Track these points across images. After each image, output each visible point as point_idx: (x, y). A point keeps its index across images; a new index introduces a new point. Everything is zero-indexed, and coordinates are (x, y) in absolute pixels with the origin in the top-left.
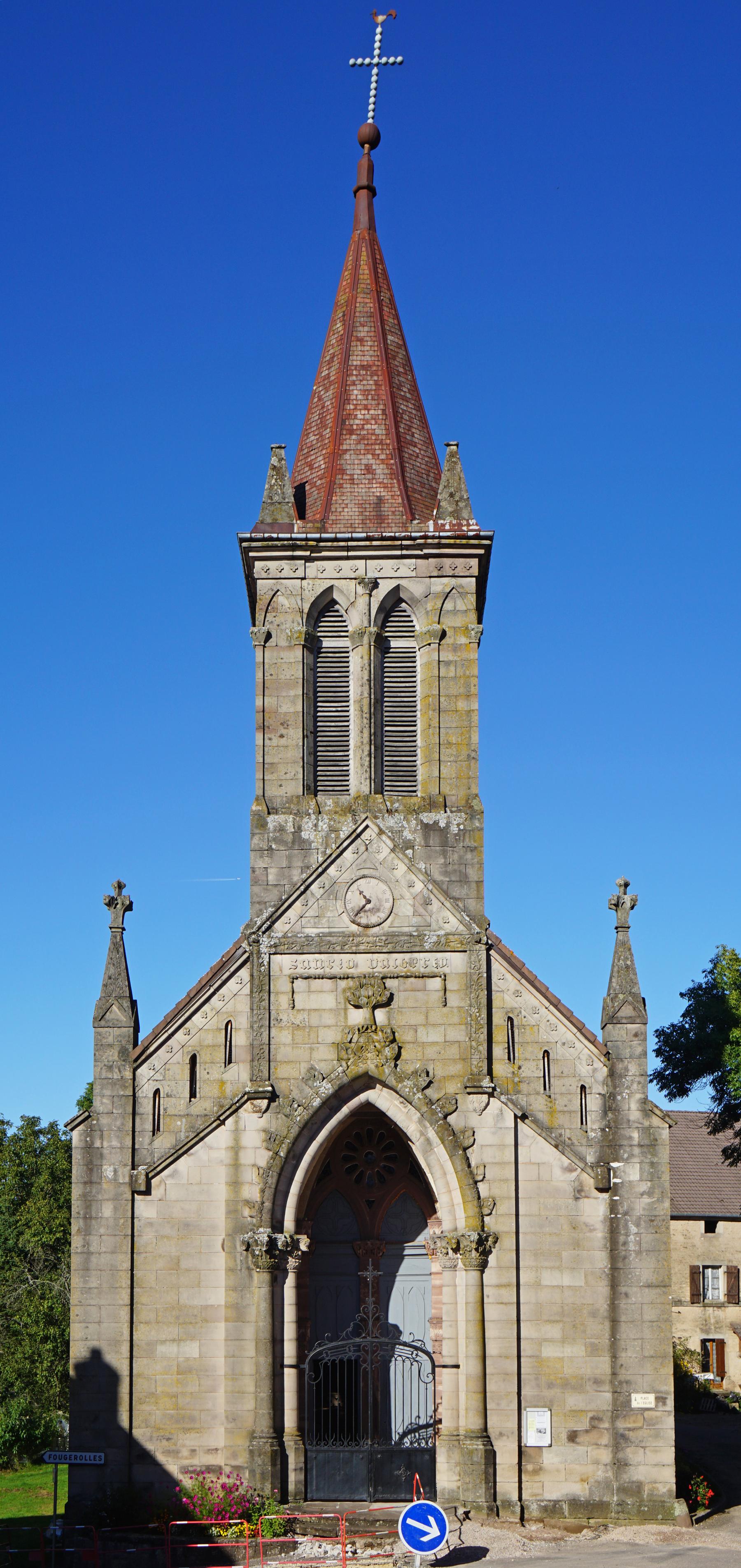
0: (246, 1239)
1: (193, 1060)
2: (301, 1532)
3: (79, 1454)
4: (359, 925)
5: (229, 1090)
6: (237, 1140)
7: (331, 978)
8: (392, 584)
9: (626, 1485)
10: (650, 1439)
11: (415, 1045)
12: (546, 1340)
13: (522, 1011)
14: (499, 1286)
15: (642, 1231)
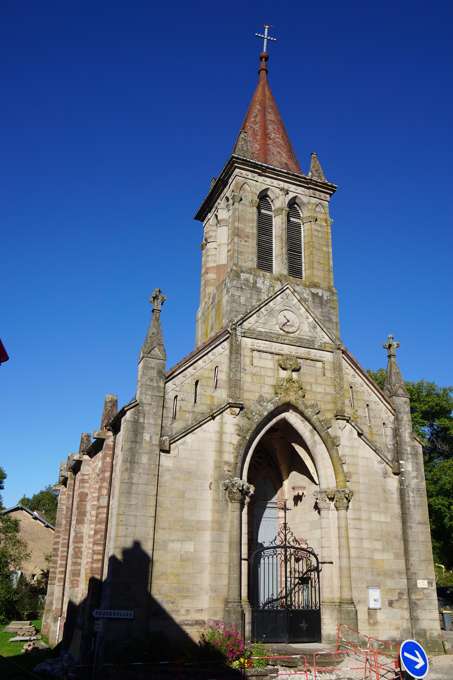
0: (226, 483)
1: (197, 383)
2: (273, 664)
3: (116, 611)
4: (284, 331)
5: (216, 401)
6: (221, 428)
7: (271, 353)
8: (295, 195)
9: (419, 631)
10: (427, 605)
11: (311, 392)
12: (375, 550)
13: (356, 385)
14: (354, 519)
15: (415, 495)
